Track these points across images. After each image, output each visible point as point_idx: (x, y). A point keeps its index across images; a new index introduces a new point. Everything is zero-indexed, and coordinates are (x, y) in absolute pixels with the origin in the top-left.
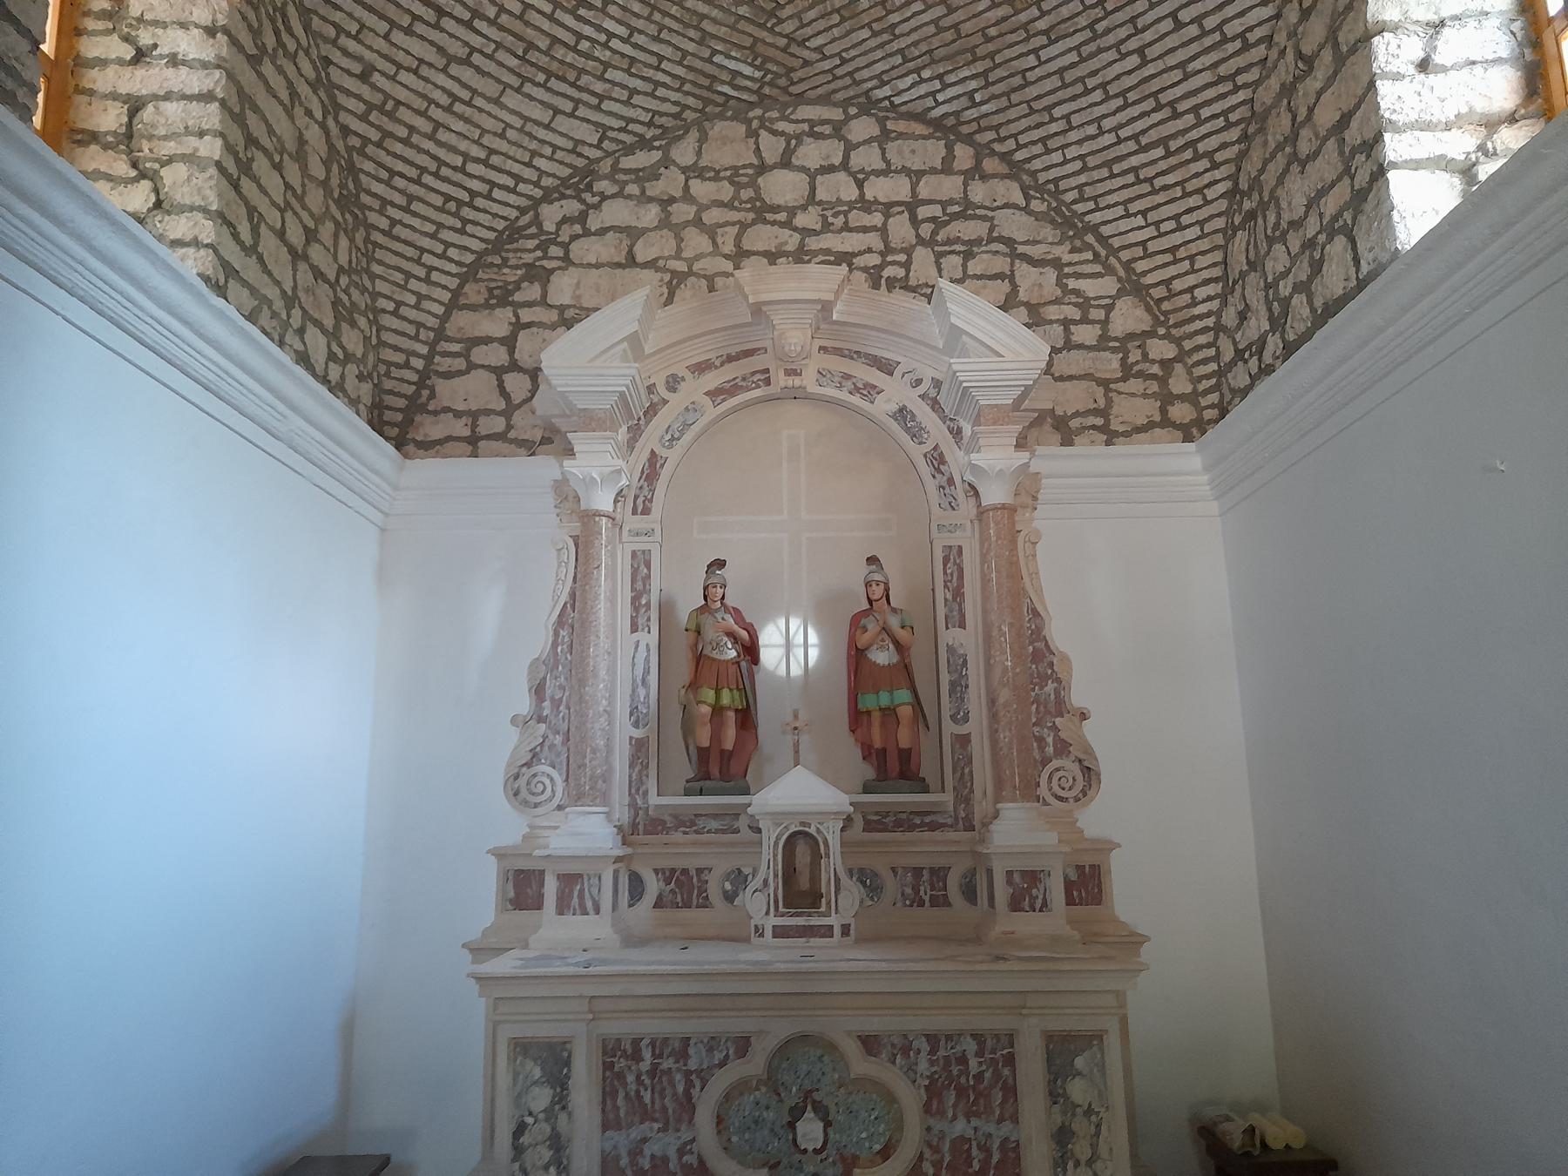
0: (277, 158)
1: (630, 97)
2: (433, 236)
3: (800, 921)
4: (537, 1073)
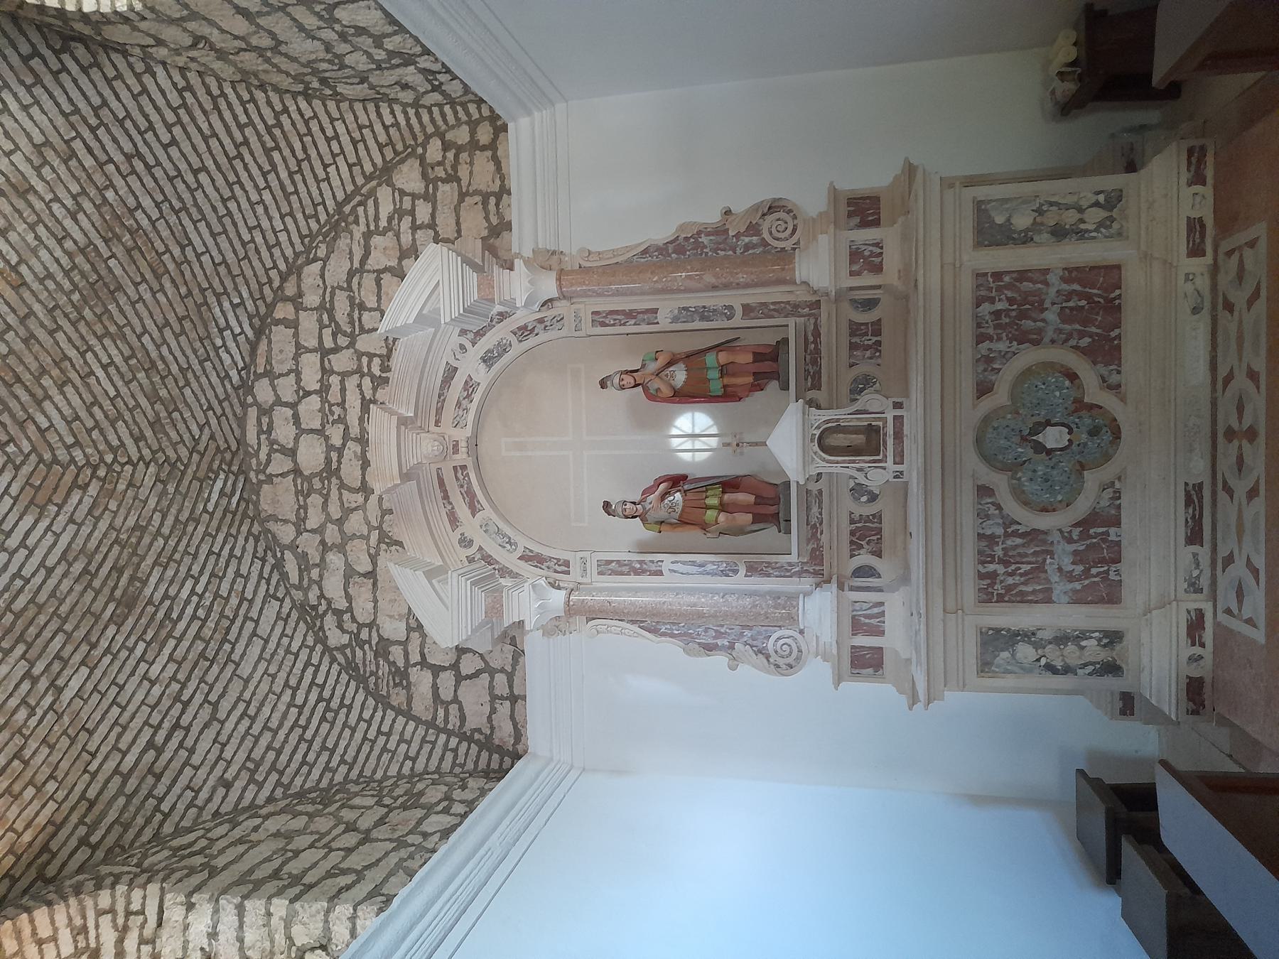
0: (290, 854)
1: (242, 576)
2: (354, 730)
3: (890, 442)
4: (1005, 655)
